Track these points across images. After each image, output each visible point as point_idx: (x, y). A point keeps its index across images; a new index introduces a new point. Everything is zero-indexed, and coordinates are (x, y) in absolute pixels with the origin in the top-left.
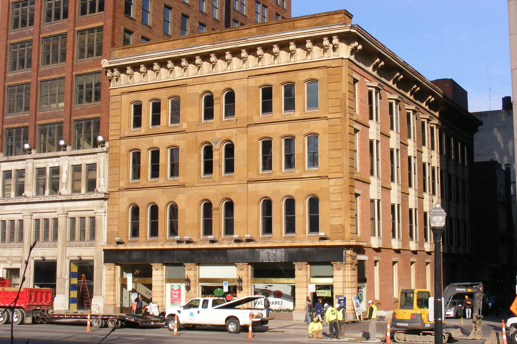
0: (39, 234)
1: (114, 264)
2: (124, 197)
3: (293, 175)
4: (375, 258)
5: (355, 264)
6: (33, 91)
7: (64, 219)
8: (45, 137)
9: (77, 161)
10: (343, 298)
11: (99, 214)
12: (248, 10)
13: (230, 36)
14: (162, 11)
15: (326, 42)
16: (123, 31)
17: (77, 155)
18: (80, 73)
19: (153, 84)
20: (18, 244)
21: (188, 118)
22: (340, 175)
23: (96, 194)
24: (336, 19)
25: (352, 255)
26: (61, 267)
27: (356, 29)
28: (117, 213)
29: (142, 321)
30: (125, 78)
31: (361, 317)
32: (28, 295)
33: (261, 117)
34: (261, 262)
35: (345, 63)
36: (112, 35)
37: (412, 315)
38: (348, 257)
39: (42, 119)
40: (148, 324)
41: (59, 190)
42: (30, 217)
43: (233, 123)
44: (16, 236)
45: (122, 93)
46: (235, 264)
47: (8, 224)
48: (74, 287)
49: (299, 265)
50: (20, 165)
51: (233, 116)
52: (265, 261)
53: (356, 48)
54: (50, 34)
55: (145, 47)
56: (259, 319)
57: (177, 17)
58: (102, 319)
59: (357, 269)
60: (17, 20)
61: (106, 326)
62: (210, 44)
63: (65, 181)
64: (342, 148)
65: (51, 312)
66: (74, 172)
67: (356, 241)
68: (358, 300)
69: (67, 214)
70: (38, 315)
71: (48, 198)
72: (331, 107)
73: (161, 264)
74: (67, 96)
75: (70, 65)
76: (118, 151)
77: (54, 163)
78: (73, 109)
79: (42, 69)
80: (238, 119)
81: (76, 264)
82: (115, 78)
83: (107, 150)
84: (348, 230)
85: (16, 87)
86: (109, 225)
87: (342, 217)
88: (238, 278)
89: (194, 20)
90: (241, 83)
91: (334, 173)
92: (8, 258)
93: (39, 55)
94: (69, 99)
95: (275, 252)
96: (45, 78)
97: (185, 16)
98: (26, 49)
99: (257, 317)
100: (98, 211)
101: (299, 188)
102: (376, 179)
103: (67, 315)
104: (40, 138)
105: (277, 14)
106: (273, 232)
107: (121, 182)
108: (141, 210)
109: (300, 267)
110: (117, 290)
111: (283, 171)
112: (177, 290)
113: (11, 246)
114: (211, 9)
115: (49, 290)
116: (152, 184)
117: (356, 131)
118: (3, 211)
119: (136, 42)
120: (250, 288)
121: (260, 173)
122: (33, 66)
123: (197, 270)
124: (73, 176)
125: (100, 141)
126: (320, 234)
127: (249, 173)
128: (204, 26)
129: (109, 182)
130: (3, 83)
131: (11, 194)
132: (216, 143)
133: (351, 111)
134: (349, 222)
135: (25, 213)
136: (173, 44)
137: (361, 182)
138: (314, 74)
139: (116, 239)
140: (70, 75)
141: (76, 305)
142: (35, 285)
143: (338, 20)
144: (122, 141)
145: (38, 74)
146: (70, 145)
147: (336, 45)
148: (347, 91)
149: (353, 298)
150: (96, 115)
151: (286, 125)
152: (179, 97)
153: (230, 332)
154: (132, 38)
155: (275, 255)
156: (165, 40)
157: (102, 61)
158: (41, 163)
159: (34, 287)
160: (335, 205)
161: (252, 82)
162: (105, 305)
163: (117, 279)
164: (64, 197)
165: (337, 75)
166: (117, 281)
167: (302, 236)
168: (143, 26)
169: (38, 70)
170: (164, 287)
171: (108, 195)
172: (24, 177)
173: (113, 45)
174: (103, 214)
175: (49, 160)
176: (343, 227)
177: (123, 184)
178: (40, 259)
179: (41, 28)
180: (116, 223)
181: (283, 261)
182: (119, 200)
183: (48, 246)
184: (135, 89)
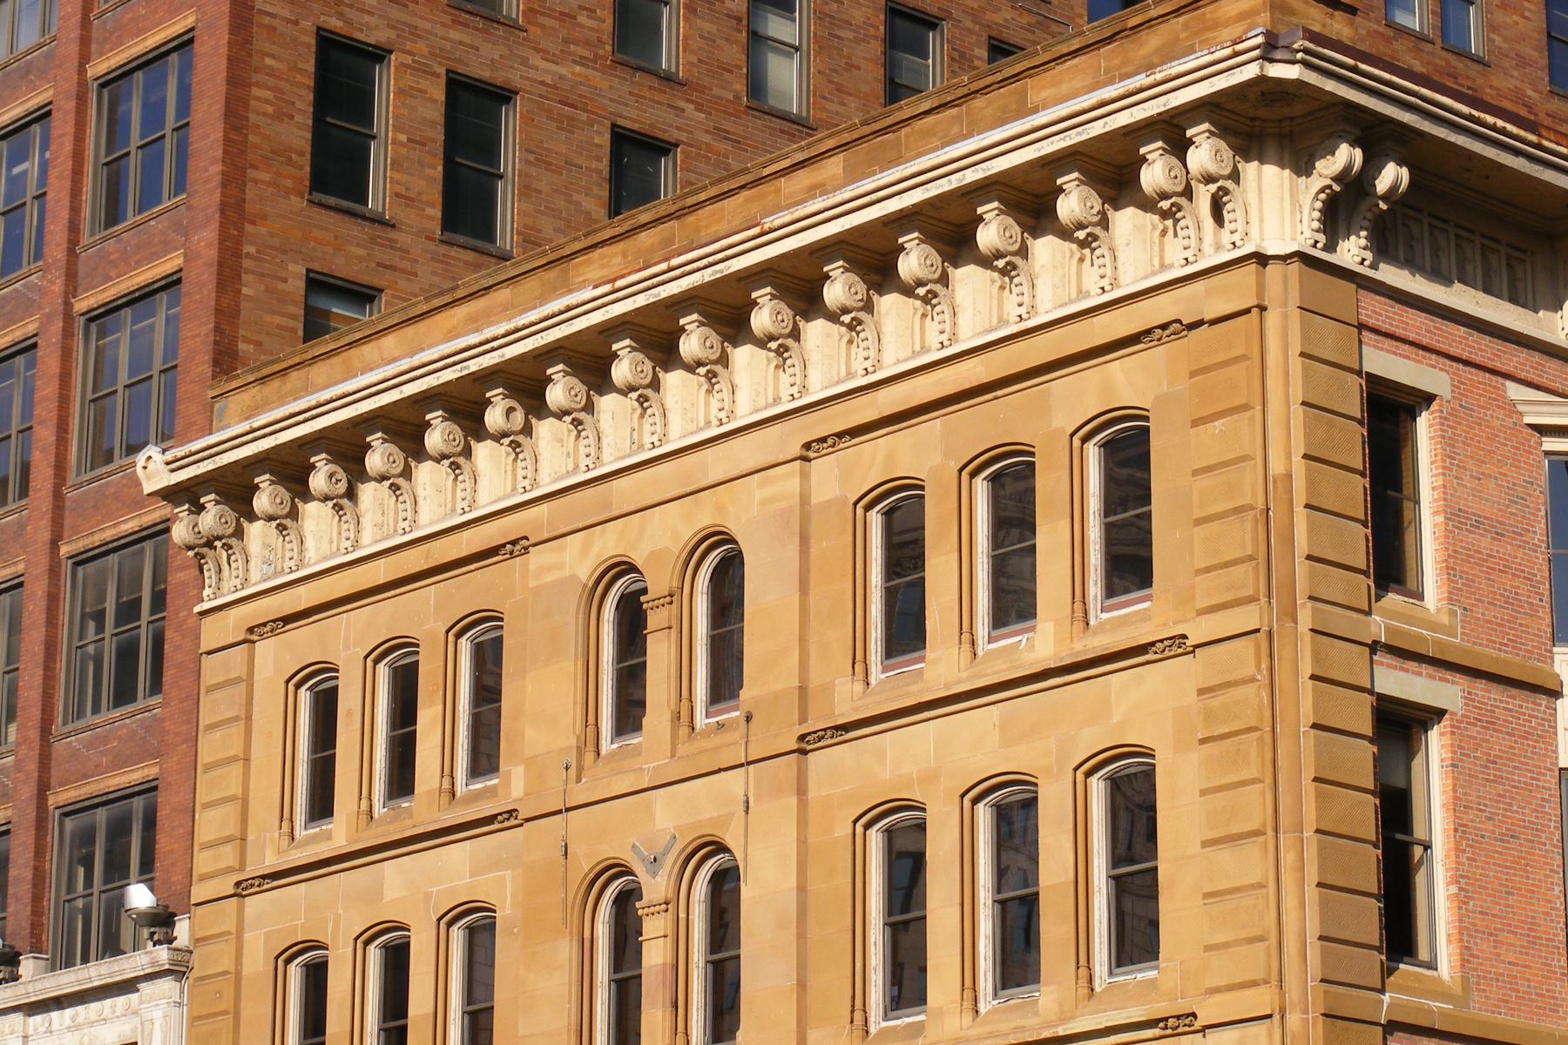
14: (594, 165)
16: (298, 286)
21: (530, 733)
22: (1260, 1000)
27: (1299, 56)
30: (266, 546)
36: (218, 311)
45: (251, 630)
51: (732, 703)
55: (354, 353)
64: (1265, 825)
72: (1207, 570)
83: (173, 962)
90: (769, 491)
91: (1230, 988)
144: (254, 904)
146: (36, 948)
148: (1297, 459)
150: (146, 772)
152: (495, 618)
156: (437, 302)
168: (455, 252)
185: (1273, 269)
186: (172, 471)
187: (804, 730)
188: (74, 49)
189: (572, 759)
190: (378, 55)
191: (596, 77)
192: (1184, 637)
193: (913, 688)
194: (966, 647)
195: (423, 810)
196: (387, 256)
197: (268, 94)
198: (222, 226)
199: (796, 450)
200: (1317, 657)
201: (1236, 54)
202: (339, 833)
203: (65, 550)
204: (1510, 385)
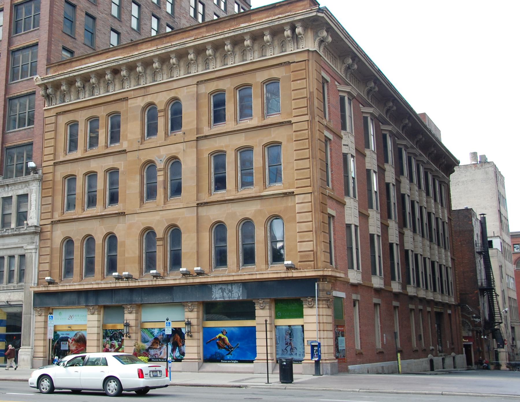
4: (354, 297)
11: (29, 251)
21: (129, 135)
22: (310, 189)
34: (213, 300)
52: (218, 300)
80: (185, 133)
87: (313, 241)
90: (188, 90)
101: (259, 208)
106: (228, 263)
108: (77, 244)
126: (286, 262)
138: (275, 73)
160: (304, 227)
174: (34, 251)
181: (241, 298)
183: (12, 288)
185: (311, 54)
186: (42, 80)
187: (198, 136)
192: (126, 150)
194: (236, 122)
195: (99, 149)
196: (74, 45)
199: (196, 83)
201: (312, 10)
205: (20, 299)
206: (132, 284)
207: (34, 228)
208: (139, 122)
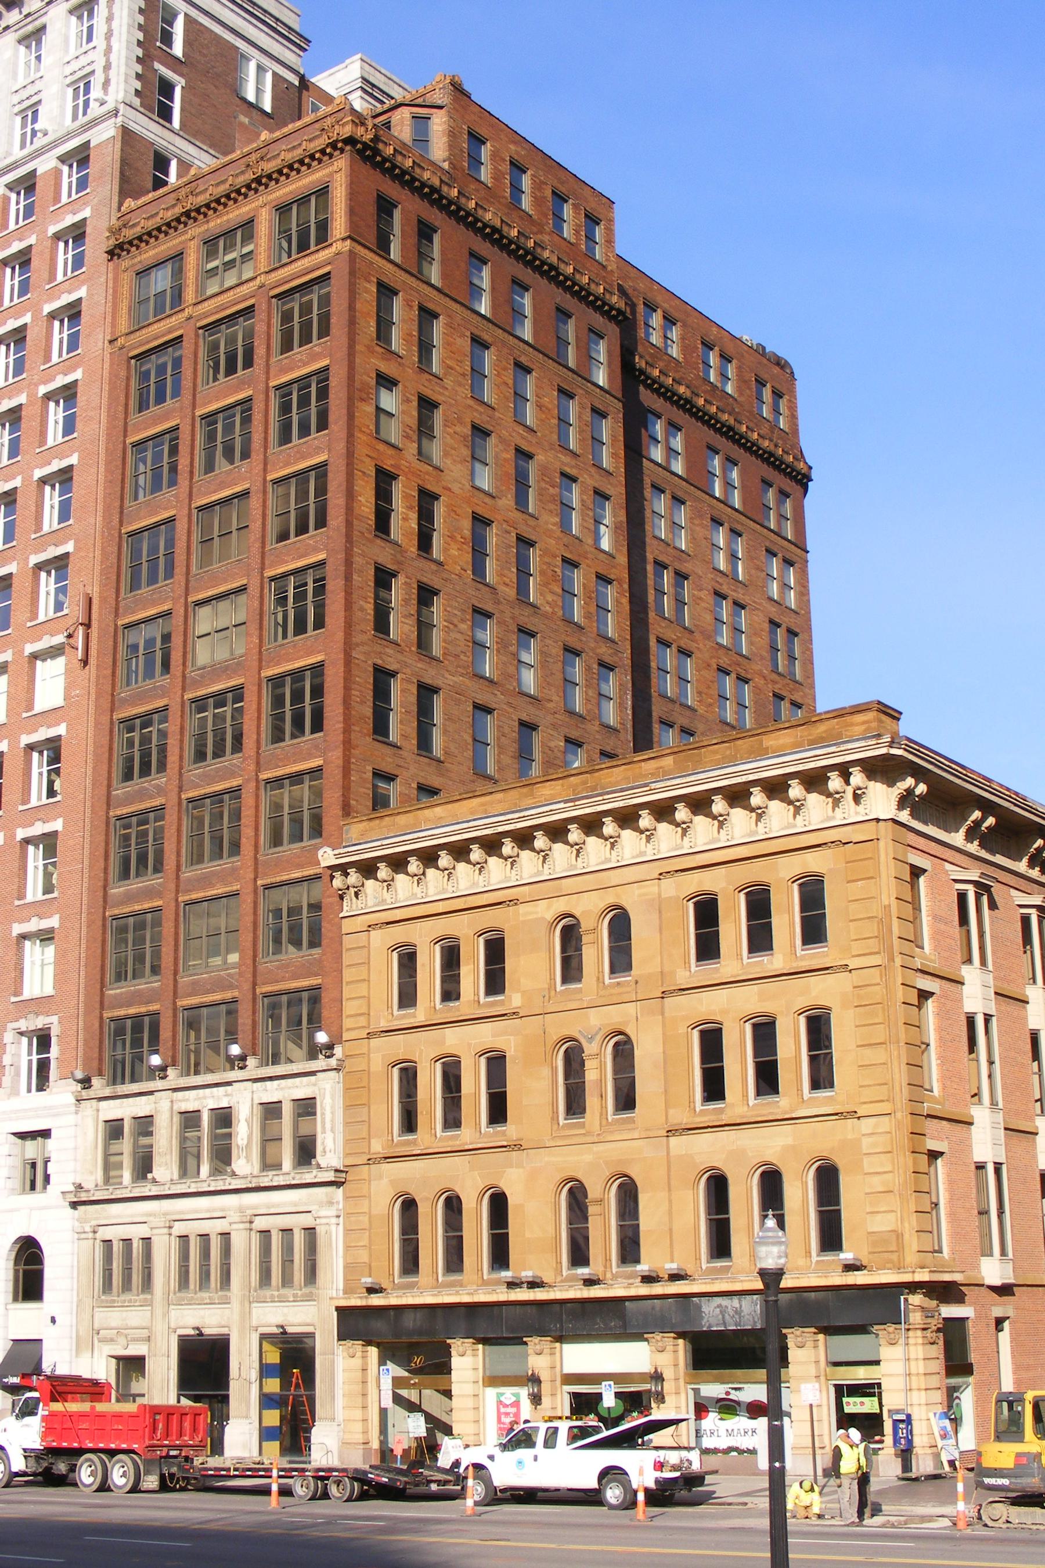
0: (187, 1272)
1: (360, 1342)
2: (381, 1177)
3: (775, 1111)
4: (998, 1312)
5: (935, 1328)
6: (168, 927)
7: (245, 1234)
8: (198, 1037)
9: (271, 1092)
10: (903, 1417)
12: (700, 693)
13: (613, 779)
15: (835, 782)
17: (271, 1079)
18: (273, 880)
19: (441, 903)
20: (142, 1296)
21: (522, 980)
22: (886, 1108)
23: (315, 1172)
24: (857, 724)
25: (925, 1306)
26: (240, 1352)
28: (366, 1219)
29: (406, 1483)
30: (375, 890)
31: (957, 1463)
32: (147, 1423)
33: (694, 972)
35: (886, 831)
37: (1019, 1456)
38: (914, 1311)
39: (190, 995)
40: (422, 1489)
41: (230, 1165)
42: (166, 1231)
43: (629, 989)
44: (136, 1278)
46: (646, 1336)
47: (117, 1247)
48: (272, 1399)
49: (797, 1336)
50: (141, 1107)
52: (715, 1329)
53: (910, 792)
54: (203, 792)
55: (419, 812)
56: (677, 1474)
57: (507, 730)
58: (317, 1478)
59: (941, 1342)
60: (130, 760)
61: (325, 1496)
62: (566, 802)
63: (245, 1142)
65: (200, 1461)
66: (266, 1119)
67: (931, 1272)
68: (947, 1421)
69: (251, 1222)
70: (174, 1470)
71: (205, 1185)
73: (471, 1340)
74: (246, 938)
75: (251, 863)
76: (364, 1067)
77: (219, 1099)
78: (261, 968)
79: (186, 874)
81: (273, 1343)
82: (352, 890)
84: (912, 1243)
85: (131, 919)
86: (347, 1247)
88: (653, 1371)
89: (552, 732)
91: (871, 1102)
92: (119, 1331)
93: (179, 842)
94: (249, 944)
95: (738, 1306)
96: (194, 896)
97: (528, 727)
98: (150, 827)
99: (674, 1468)
100: (322, 1213)
102: (988, 1111)
103: (236, 1469)
104: (188, 1040)
105: (775, 695)
107: (373, 1141)
108: (423, 1209)
109: (799, 1339)
110: (370, 1405)
111: (751, 1103)
112: (512, 1405)
113: (125, 1301)
114: (594, 701)
115: (200, 1408)
116: (446, 1144)
117: (924, 995)
118: (106, 1218)
119: (405, 799)
120: (683, 1396)
121: (698, 1110)
122: (166, 867)
123: (558, 1354)
124: (263, 1129)
125: (322, 1044)
127: (671, 1112)
128: (579, 745)
129: (347, 1142)
130: (101, 910)
131: (122, 1176)
132: (590, 1040)
133: (907, 947)
134: (912, 1222)
135: (155, 1221)
136: (483, 805)
137: (944, 1122)
138: (813, 862)
139: (363, 1280)
140: (250, 888)
141: (276, 1444)
142: (182, 1398)
143: (863, 727)
144: (374, 1042)
145: (177, 886)
146: (254, 1054)
147: (860, 789)
148: (893, 899)
149: (931, 1415)
151: (752, 990)
153: (612, 1507)
154: (394, 791)
155: (738, 1312)
156: (465, 796)
157: (320, 853)
158: (189, 1101)
159: (179, 1401)
160: (877, 1183)
161: (670, 888)
162: (345, 1444)
163: (369, 1380)
164: (242, 1181)
165: (866, 862)
166: (369, 1384)
167: (801, 1262)
168: (422, 759)
169: (178, 877)
170: (481, 1396)
171: (344, 1175)
172: (150, 1134)
173: (347, 810)
174: (334, 1220)
175: (208, 1091)
176: (899, 1236)
177: (378, 1147)
178: (192, 1332)
179: (184, 778)
180: (365, 1242)
181: (759, 1327)
182: (369, 1184)
184: (399, 915)
185: (881, 823)
188: (256, 664)
189: (546, 993)
190: (393, 674)
191: (467, 681)
193: (715, 976)
197: (357, 693)
198: (344, 750)
200: (903, 976)
202: (420, 1014)
203: (259, 882)
204: (1012, 890)
205: (308, 1321)
206: (539, 1295)
207: (332, 1173)
208: (544, 955)
